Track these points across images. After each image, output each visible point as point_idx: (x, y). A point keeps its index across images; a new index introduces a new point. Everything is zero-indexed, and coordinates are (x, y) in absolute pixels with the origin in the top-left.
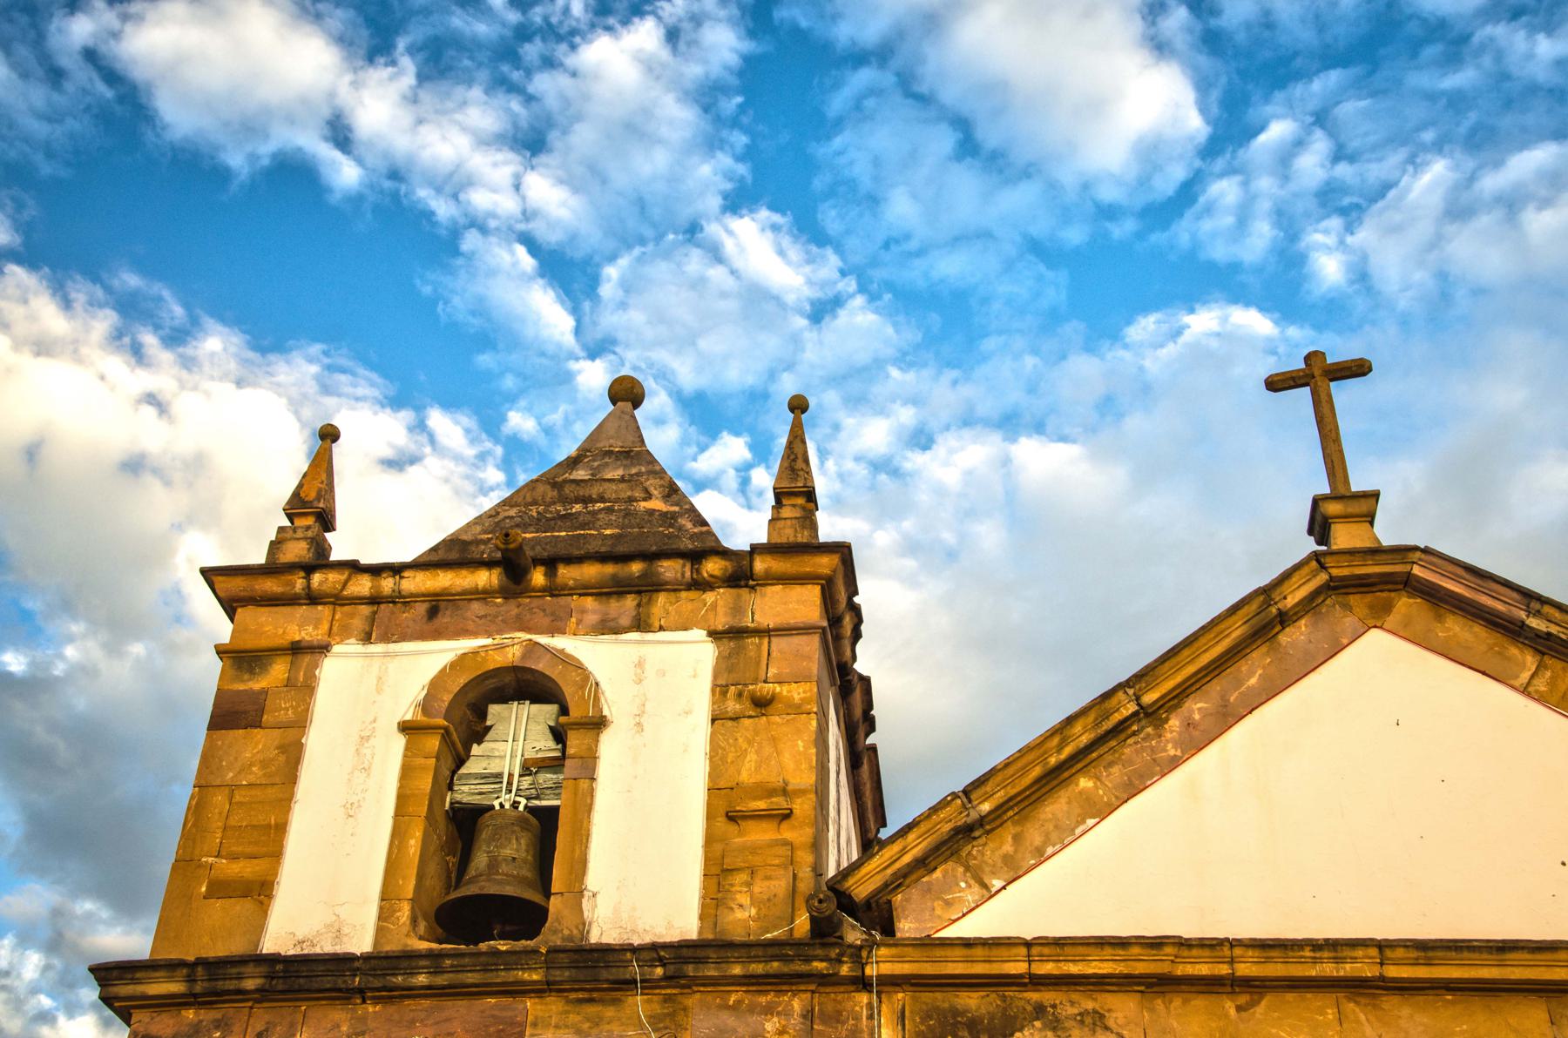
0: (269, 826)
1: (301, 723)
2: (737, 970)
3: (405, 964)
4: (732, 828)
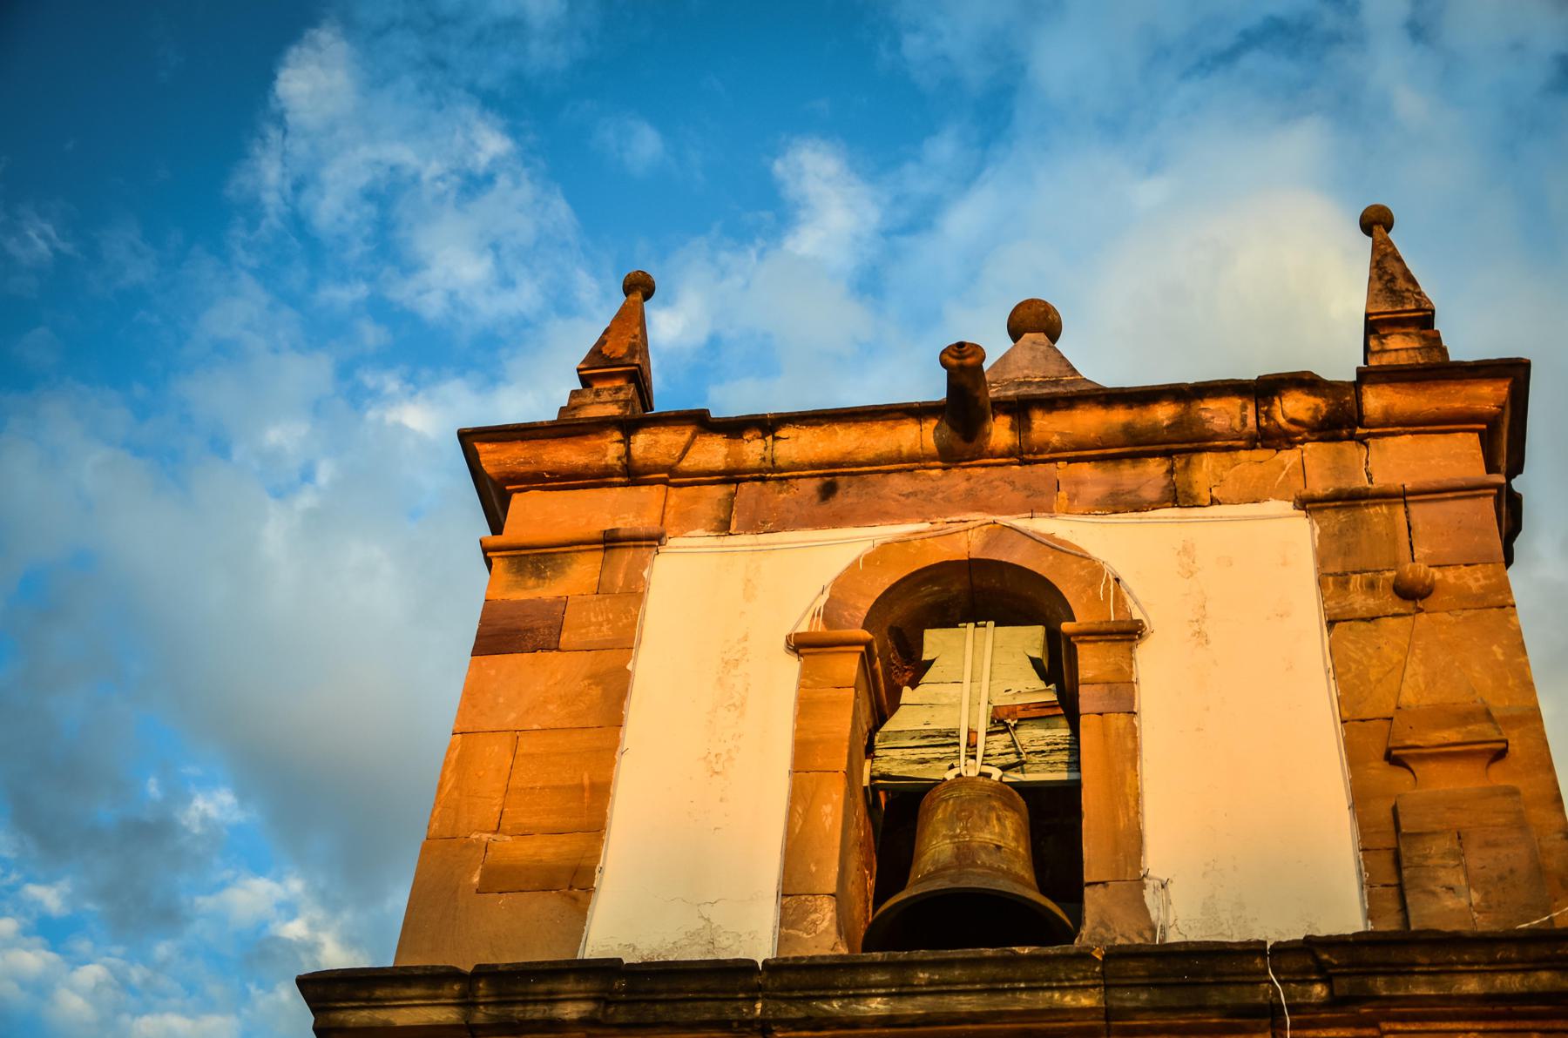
0: (581, 787)
1: (624, 643)
2: (1471, 986)
3: (844, 979)
4: (1400, 777)
